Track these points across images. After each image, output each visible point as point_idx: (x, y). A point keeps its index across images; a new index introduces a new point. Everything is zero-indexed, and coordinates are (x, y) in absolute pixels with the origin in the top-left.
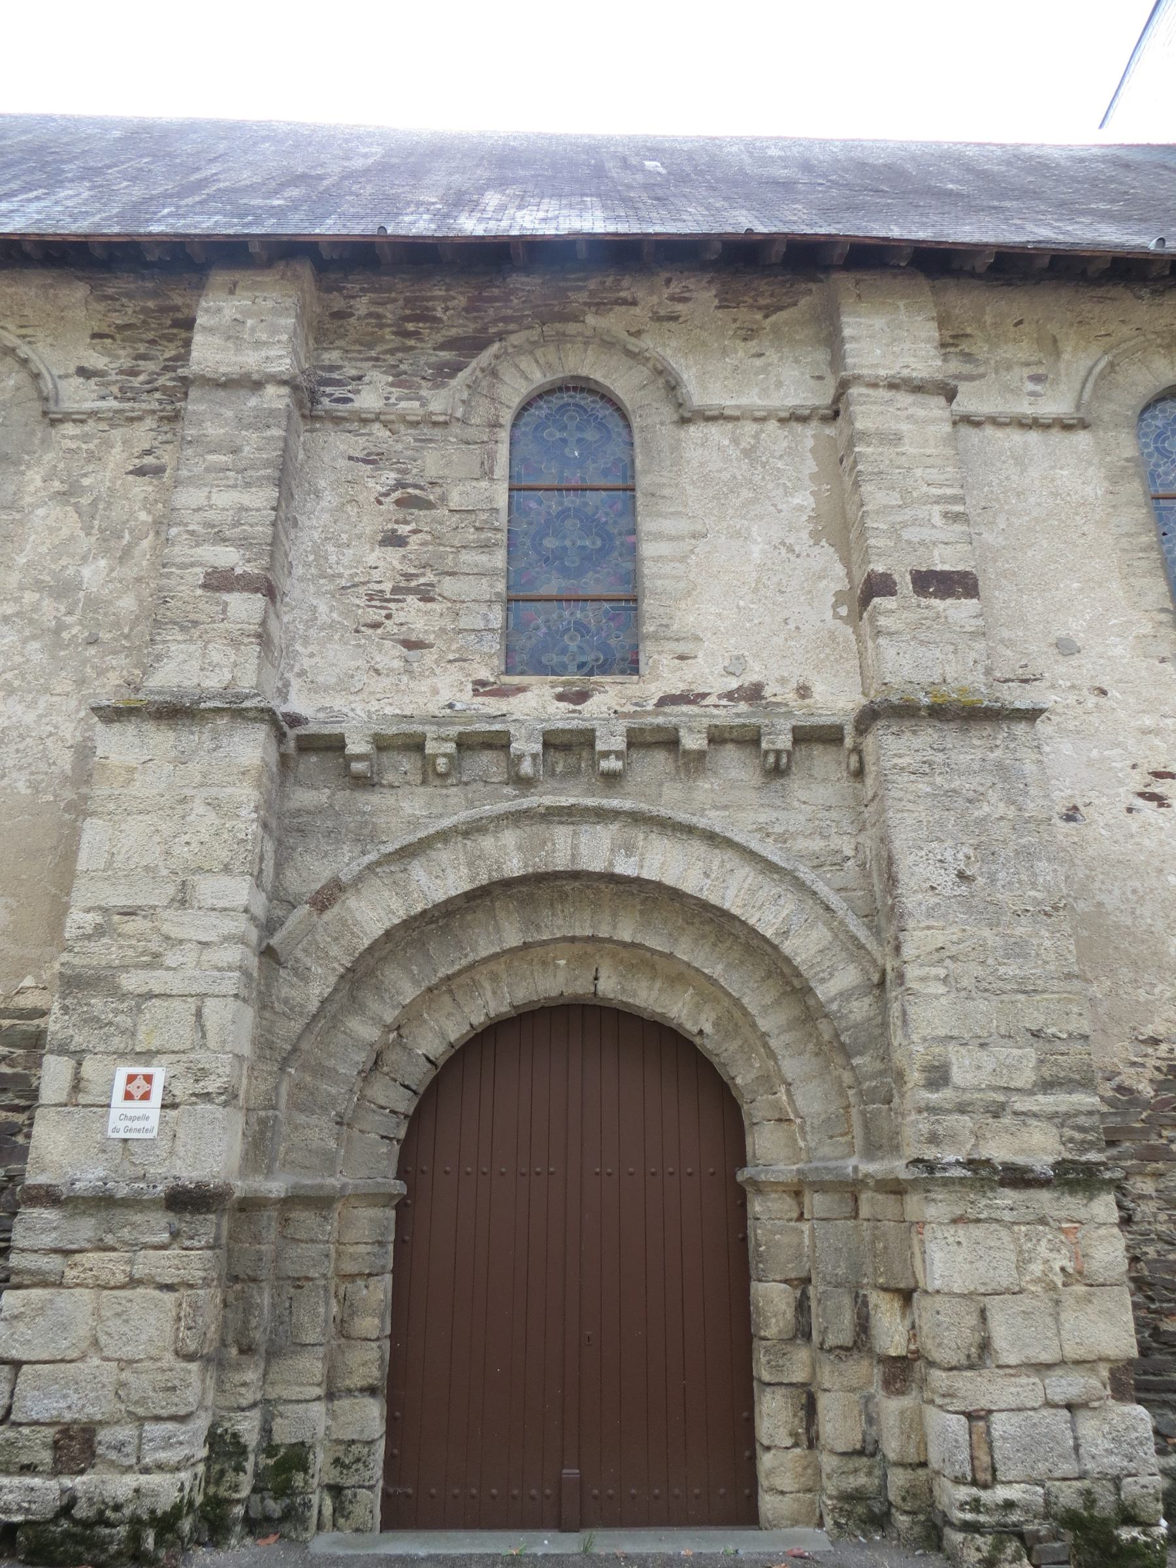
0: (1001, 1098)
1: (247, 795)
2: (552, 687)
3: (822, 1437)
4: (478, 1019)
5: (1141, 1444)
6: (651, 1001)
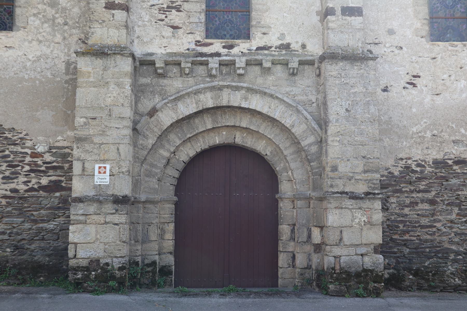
1: (127, 81)
2: (221, 43)
3: (296, 265)
4: (199, 150)
5: (380, 264)
6: (251, 145)
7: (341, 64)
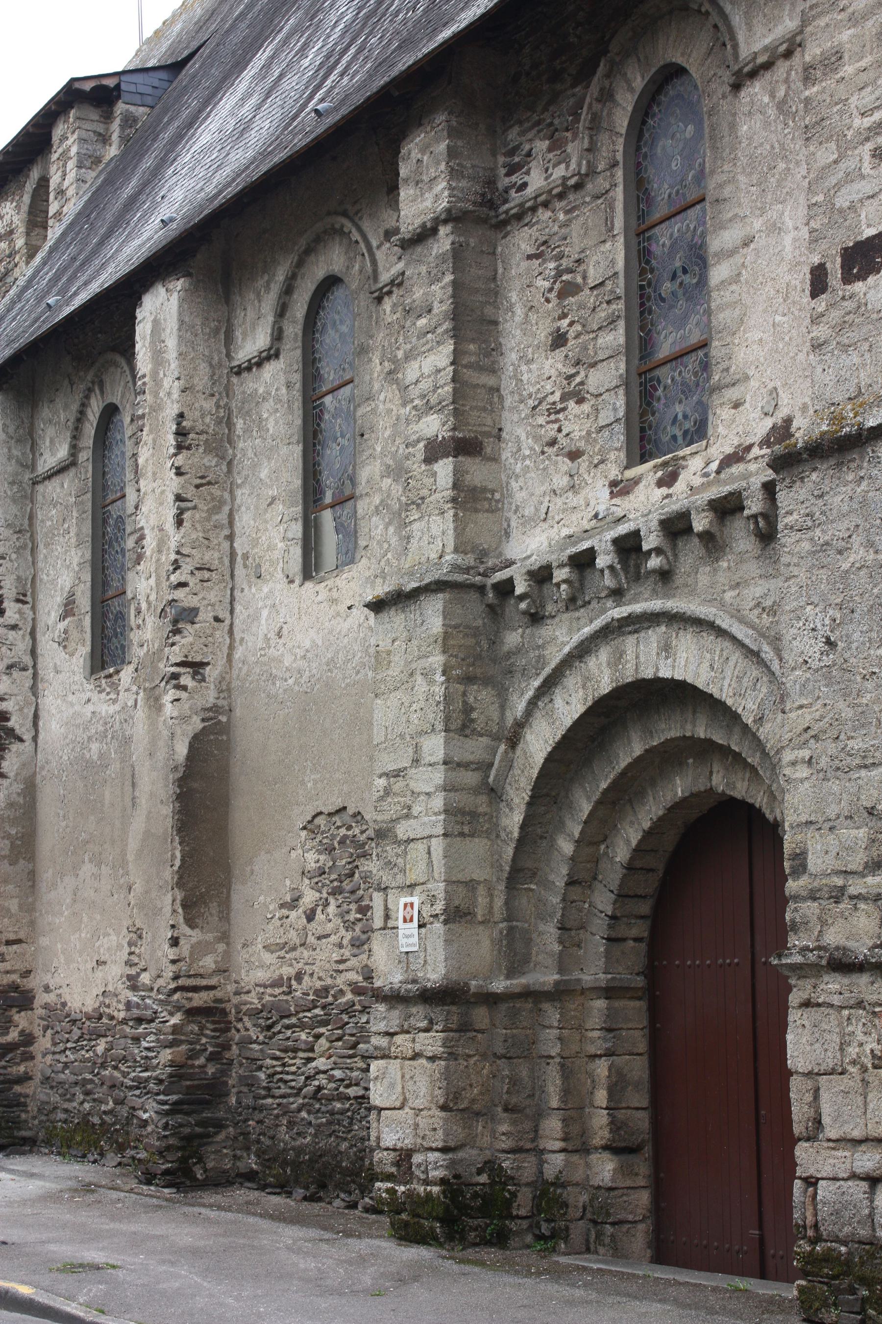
0: (839, 881)
7: (814, 476)
